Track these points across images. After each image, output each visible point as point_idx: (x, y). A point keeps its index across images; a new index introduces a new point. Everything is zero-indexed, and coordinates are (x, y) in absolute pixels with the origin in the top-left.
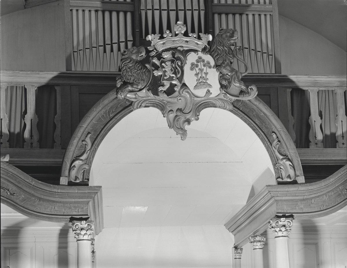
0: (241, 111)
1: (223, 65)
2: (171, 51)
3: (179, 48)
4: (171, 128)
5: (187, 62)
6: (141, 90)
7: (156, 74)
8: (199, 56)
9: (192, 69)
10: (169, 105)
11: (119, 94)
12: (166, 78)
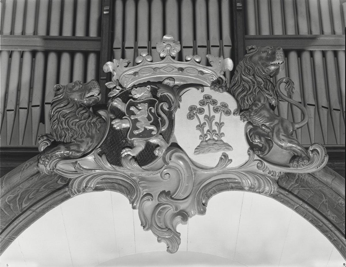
0: (296, 196)
1: (254, 108)
2: (149, 86)
3: (166, 82)
4: (146, 228)
5: (181, 104)
6: (85, 155)
7: (118, 126)
8: (205, 95)
9: (190, 117)
10: (143, 185)
11: (41, 162)
12: (136, 132)
